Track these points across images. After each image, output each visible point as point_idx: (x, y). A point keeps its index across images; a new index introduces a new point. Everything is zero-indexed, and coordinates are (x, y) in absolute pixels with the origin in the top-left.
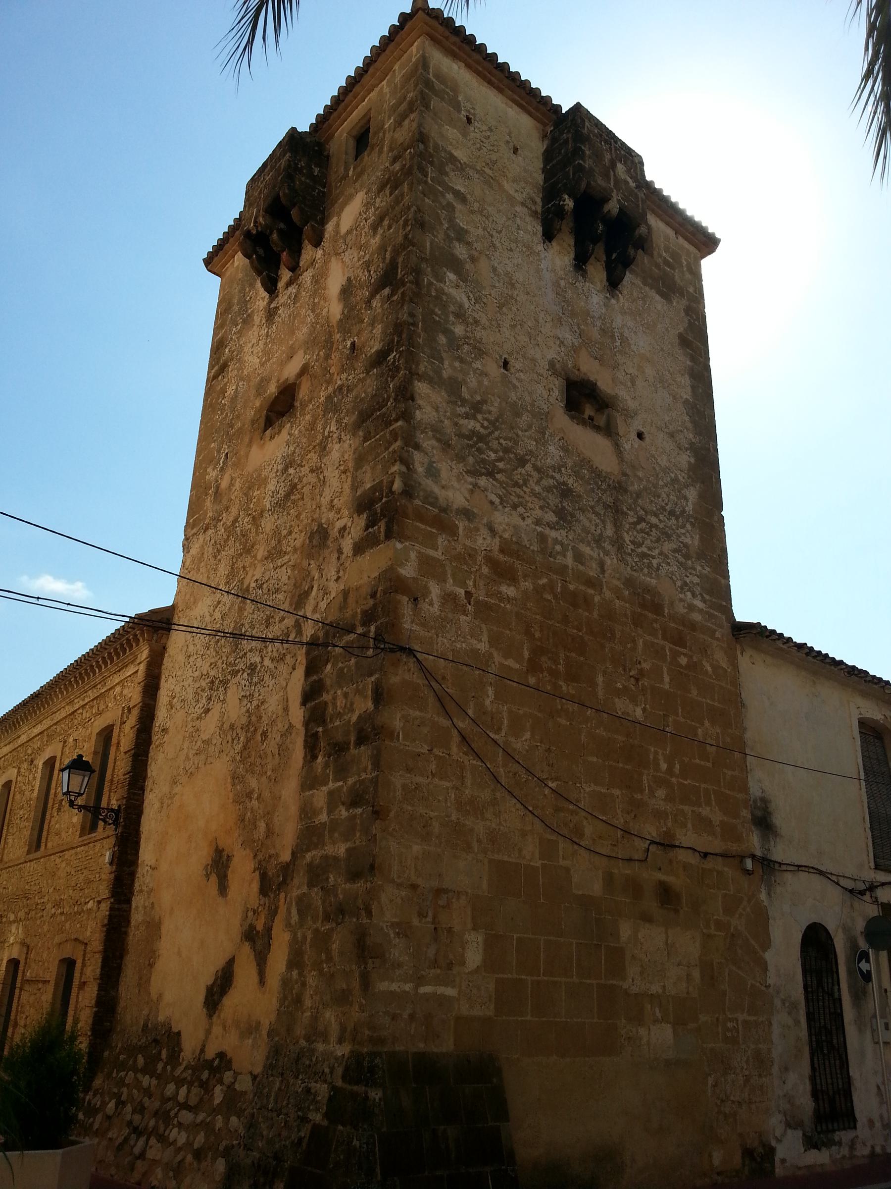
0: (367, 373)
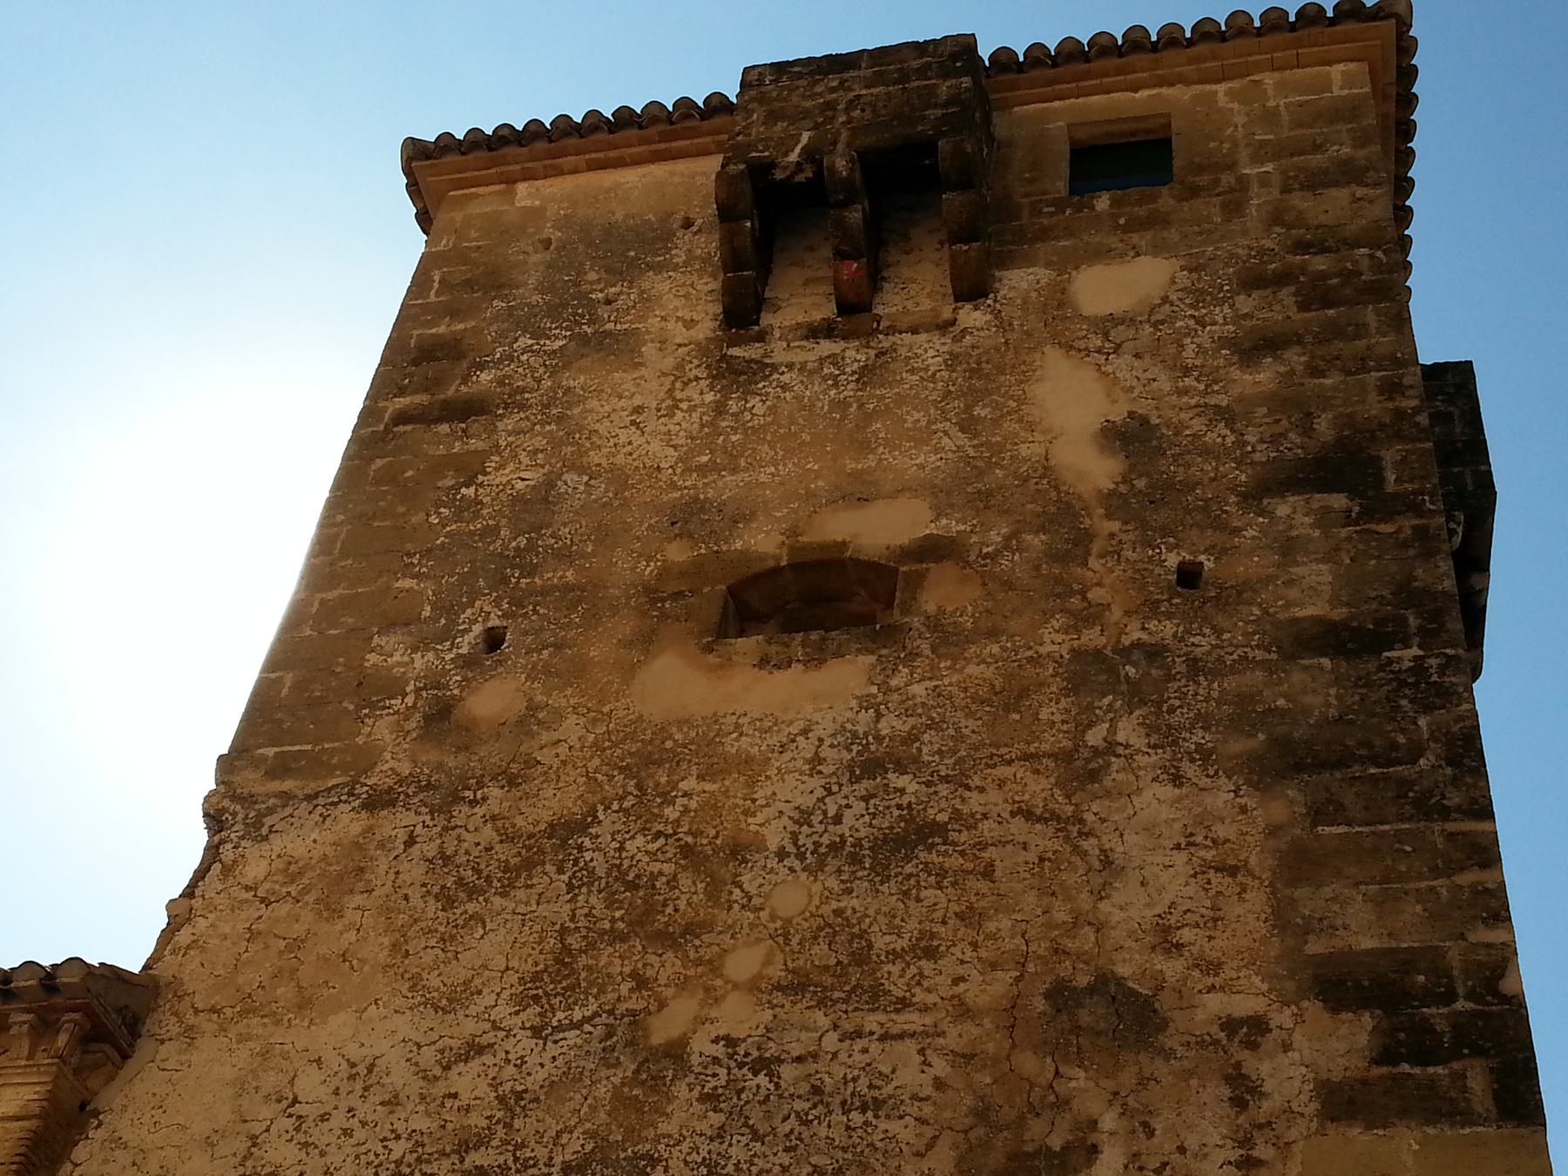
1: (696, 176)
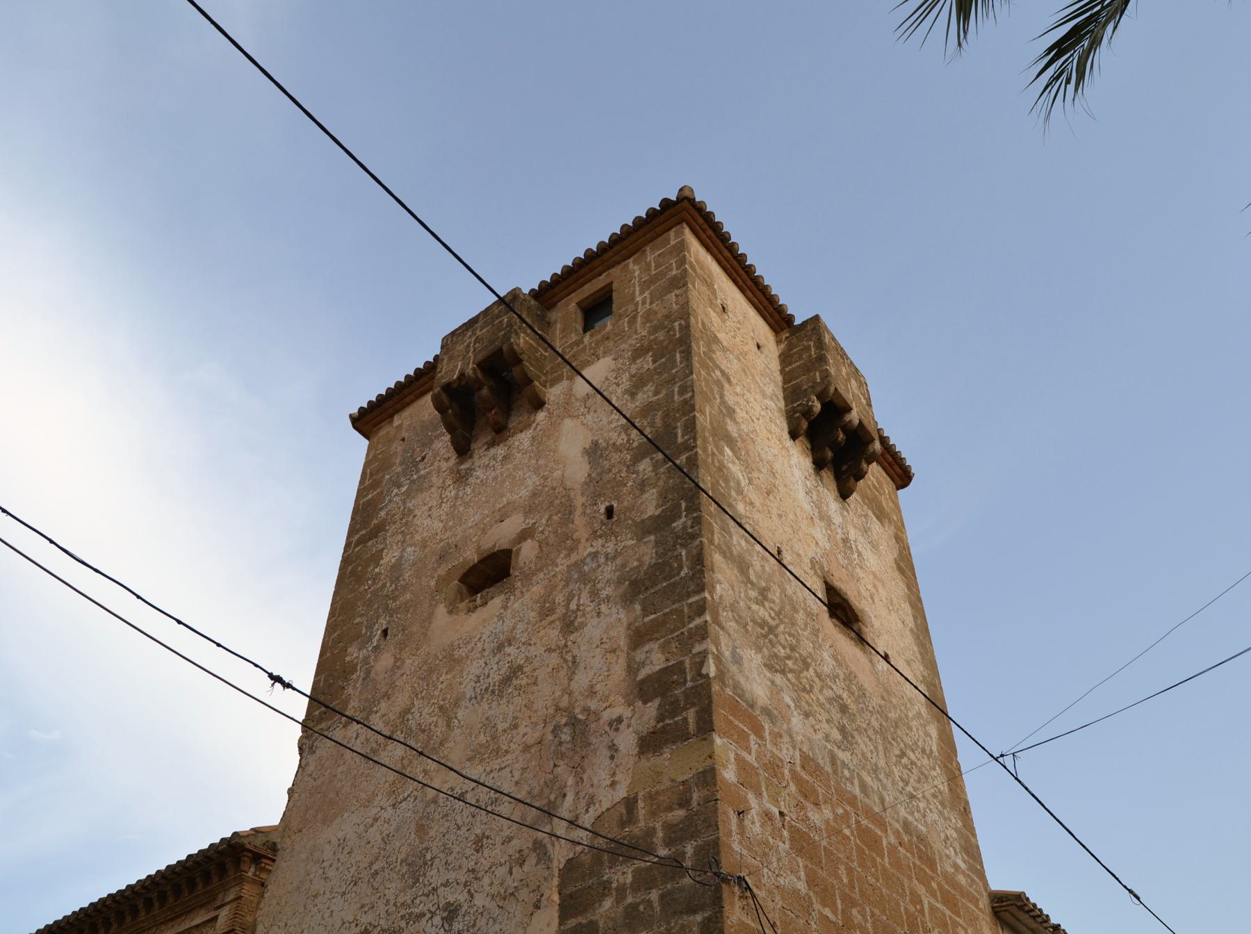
0: (640, 540)
1: (425, 409)
